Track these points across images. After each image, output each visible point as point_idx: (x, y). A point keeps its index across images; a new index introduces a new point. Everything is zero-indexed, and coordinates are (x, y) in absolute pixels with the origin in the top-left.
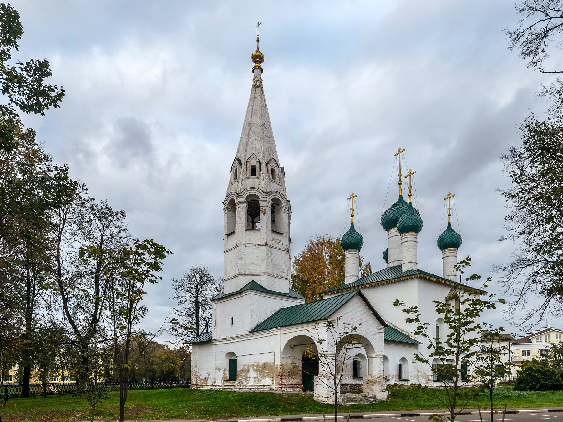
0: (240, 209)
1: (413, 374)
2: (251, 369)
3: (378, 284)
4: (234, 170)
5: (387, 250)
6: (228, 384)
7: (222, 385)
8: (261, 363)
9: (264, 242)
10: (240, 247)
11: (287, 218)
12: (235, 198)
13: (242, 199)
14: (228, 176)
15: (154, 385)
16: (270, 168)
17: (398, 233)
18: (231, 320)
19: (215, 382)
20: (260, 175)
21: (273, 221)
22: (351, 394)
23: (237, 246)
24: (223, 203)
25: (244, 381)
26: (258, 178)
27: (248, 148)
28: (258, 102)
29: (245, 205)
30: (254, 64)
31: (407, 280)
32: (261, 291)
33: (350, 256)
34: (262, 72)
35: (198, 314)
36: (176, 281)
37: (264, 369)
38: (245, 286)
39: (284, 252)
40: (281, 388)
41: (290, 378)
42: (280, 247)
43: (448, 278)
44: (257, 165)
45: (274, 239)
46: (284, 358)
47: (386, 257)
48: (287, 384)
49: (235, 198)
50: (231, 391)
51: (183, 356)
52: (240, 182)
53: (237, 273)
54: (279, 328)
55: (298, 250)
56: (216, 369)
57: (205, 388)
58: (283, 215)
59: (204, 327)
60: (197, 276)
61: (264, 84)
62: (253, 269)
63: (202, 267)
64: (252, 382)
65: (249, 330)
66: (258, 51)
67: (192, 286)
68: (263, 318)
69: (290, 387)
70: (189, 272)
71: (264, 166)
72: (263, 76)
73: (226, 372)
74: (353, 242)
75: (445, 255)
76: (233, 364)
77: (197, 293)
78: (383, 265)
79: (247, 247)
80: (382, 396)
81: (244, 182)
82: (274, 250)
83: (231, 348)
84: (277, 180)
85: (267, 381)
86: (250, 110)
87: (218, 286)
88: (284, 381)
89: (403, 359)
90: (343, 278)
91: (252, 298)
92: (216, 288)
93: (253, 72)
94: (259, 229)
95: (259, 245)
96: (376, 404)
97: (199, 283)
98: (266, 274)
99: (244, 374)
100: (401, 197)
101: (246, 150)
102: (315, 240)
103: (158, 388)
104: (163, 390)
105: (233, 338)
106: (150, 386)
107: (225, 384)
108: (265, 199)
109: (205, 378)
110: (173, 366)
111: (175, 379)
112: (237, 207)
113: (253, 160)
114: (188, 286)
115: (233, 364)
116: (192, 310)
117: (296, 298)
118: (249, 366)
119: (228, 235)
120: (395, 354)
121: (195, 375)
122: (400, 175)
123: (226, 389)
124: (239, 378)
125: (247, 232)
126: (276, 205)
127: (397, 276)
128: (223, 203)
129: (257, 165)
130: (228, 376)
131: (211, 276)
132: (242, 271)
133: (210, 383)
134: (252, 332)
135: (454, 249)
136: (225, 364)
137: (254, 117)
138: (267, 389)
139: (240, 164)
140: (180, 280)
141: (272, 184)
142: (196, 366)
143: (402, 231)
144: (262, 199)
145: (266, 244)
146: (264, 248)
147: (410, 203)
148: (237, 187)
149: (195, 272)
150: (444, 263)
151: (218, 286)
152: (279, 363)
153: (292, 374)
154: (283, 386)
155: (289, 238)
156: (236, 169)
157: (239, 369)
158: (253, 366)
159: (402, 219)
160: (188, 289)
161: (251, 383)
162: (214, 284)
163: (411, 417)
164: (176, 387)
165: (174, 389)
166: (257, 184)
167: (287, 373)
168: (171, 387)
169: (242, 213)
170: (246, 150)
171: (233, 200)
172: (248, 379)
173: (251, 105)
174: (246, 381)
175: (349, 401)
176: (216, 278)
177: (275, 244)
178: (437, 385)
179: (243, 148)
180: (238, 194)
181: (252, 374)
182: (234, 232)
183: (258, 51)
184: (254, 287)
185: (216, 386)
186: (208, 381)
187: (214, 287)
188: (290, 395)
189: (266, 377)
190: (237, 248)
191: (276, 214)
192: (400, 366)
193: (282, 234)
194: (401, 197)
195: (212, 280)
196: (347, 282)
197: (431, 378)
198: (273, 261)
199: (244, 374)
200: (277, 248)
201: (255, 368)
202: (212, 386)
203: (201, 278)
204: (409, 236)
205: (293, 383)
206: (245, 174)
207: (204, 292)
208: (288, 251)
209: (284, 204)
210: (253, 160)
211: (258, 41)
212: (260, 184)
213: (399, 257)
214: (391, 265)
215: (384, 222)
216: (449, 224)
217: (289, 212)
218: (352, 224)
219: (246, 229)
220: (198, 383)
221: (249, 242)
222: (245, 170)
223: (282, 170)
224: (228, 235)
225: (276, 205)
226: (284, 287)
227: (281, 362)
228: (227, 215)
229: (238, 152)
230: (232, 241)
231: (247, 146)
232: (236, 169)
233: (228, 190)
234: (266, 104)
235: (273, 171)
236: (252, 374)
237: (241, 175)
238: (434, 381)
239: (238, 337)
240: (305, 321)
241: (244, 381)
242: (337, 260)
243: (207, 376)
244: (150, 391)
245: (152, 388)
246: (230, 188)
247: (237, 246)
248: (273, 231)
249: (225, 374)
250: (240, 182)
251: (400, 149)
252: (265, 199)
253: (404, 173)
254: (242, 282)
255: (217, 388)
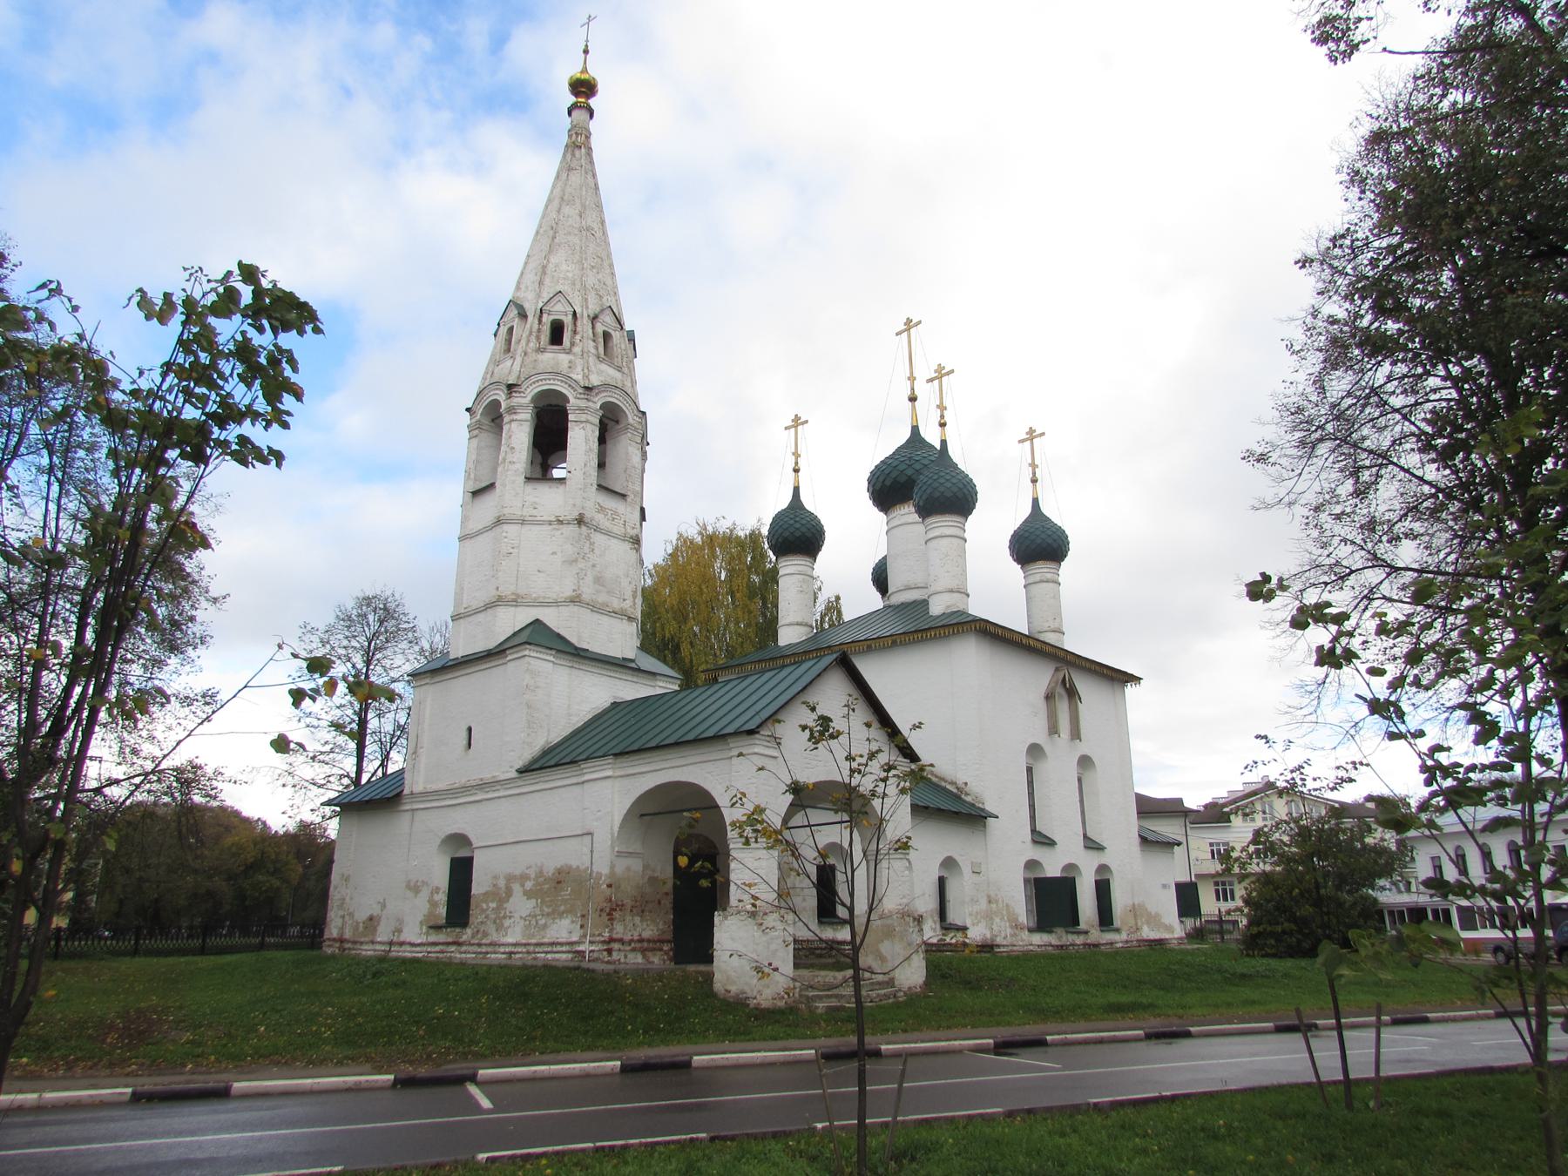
0: (514, 425)
1: (976, 908)
2: (516, 887)
3: (869, 647)
4: (503, 330)
5: (885, 558)
6: (441, 937)
7: (423, 939)
8: (550, 869)
9: (575, 514)
10: (505, 527)
11: (639, 453)
12: (501, 396)
13: (525, 398)
14: (488, 345)
15: (212, 941)
16: (600, 328)
17: (916, 517)
18: (465, 734)
19: (400, 931)
20: (573, 344)
21: (601, 465)
22: (823, 973)
23: (499, 522)
24: (468, 410)
25: (491, 928)
26: (569, 352)
27: (547, 281)
28: (576, 178)
29: (528, 416)
30: (573, 99)
31: (946, 636)
32: (559, 651)
33: (790, 569)
34: (591, 116)
35: (363, 723)
36: (313, 631)
37: (557, 888)
38: (515, 634)
39: (627, 546)
40: (610, 951)
41: (637, 920)
42: (618, 530)
43: (1043, 637)
44: (568, 320)
45: (601, 509)
46: (620, 854)
47: (880, 579)
48: (627, 937)
49: (501, 396)
50: (449, 964)
51: (306, 853)
52: (519, 360)
53: (491, 594)
54: (610, 760)
55: (656, 550)
56: (408, 887)
57: (368, 951)
58: (624, 447)
59: (378, 763)
60: (371, 618)
61: (595, 142)
62: (538, 586)
63: (388, 593)
64: (519, 931)
65: (519, 764)
66: (585, 70)
67: (354, 643)
68: (557, 731)
69: (636, 943)
70: (350, 604)
71: (584, 325)
72: (593, 126)
73: (436, 897)
74: (799, 535)
75: (1031, 580)
76: (461, 870)
77: (368, 663)
78: (875, 601)
79: (527, 527)
80: (913, 974)
81: (528, 360)
82: (599, 538)
83: (460, 820)
84: (618, 361)
85: (563, 929)
86: (558, 191)
87: (427, 646)
88: (619, 930)
89: (949, 863)
90: (770, 627)
91: (539, 665)
92: (422, 650)
93: (570, 114)
94: (562, 480)
95: (560, 522)
96: (898, 1005)
97: (376, 635)
98: (575, 600)
99: (493, 905)
100: (915, 430)
101: (541, 283)
102: (692, 532)
103: (221, 951)
104: (228, 958)
105: (466, 789)
106: (197, 943)
107: (432, 938)
108: (583, 404)
109: (371, 918)
110: (276, 883)
111: (276, 925)
112: (506, 419)
113: (559, 307)
114: (345, 643)
115: (461, 870)
116: (350, 712)
117: (654, 674)
118: (510, 879)
119: (476, 493)
120: (933, 846)
121: (341, 907)
122: (912, 379)
123: (434, 953)
124: (476, 917)
125: (530, 488)
126: (610, 423)
127: (918, 626)
128: (468, 410)
129: (568, 320)
130: (443, 911)
131: (411, 617)
132: (507, 590)
133: (383, 934)
134: (524, 771)
135: (1053, 565)
136: (440, 875)
137: (566, 210)
138: (564, 956)
139: (523, 315)
140: (322, 628)
141: (604, 367)
142: (347, 879)
143: (925, 511)
144: (574, 401)
145: (580, 521)
146: (574, 528)
147: (944, 443)
148: (511, 370)
149: (368, 605)
150: (1029, 599)
151: (427, 646)
152: (605, 871)
153: (641, 906)
154: (616, 946)
155: (642, 510)
156: (511, 329)
157: (478, 886)
158: (523, 878)
159: (919, 483)
160: (342, 652)
161: (513, 935)
162: (415, 641)
163: (1029, 1050)
164: (277, 947)
165: (268, 954)
166: (566, 364)
167: (628, 902)
168: (262, 946)
169: (519, 434)
170: (541, 283)
171: (495, 404)
172: (507, 923)
173: (560, 184)
174: (500, 928)
175: (820, 998)
176: (423, 627)
177: (604, 522)
178: (1039, 939)
179: (531, 278)
180: (510, 387)
181: (521, 906)
182: (492, 486)
183: (585, 70)
184: (538, 636)
185: (402, 944)
186: (380, 929)
187: (417, 648)
188: (640, 974)
189: (561, 915)
190: (498, 530)
191: (609, 445)
192: (942, 882)
193: (623, 496)
194: (915, 430)
195: (413, 629)
196: (782, 642)
197: (1023, 918)
198: (598, 568)
199: (493, 905)
200: (608, 533)
201: (529, 885)
202: (391, 943)
203: (381, 622)
204: (943, 524)
205: (647, 934)
206: (533, 338)
207: (387, 663)
208: (636, 541)
209: (632, 418)
210: (559, 307)
211: (586, 52)
212: (573, 369)
213: (918, 579)
214: (896, 599)
215: (878, 486)
216: (1035, 502)
217: (644, 441)
218: (796, 490)
219: (528, 479)
220: (348, 935)
221: (535, 512)
222: (536, 326)
223: (631, 337)
224: (476, 493)
225: (610, 423)
226: (622, 640)
227: (612, 867)
228: (475, 441)
229: (518, 288)
230: (488, 508)
231: (544, 273)
232: (511, 329)
233: (484, 378)
234: (596, 185)
235: (607, 336)
236: (521, 906)
237: (523, 342)
238: (1031, 930)
239: (483, 786)
240: (635, 747)
241: (491, 928)
242: (750, 585)
243: (376, 911)
244: (198, 959)
245: (202, 951)
246: (489, 372)
247: (499, 522)
248: (600, 487)
249: (434, 904)
250: (519, 360)
251: (909, 321)
252: (583, 404)
253: (924, 371)
254: (509, 621)
255: (407, 952)
